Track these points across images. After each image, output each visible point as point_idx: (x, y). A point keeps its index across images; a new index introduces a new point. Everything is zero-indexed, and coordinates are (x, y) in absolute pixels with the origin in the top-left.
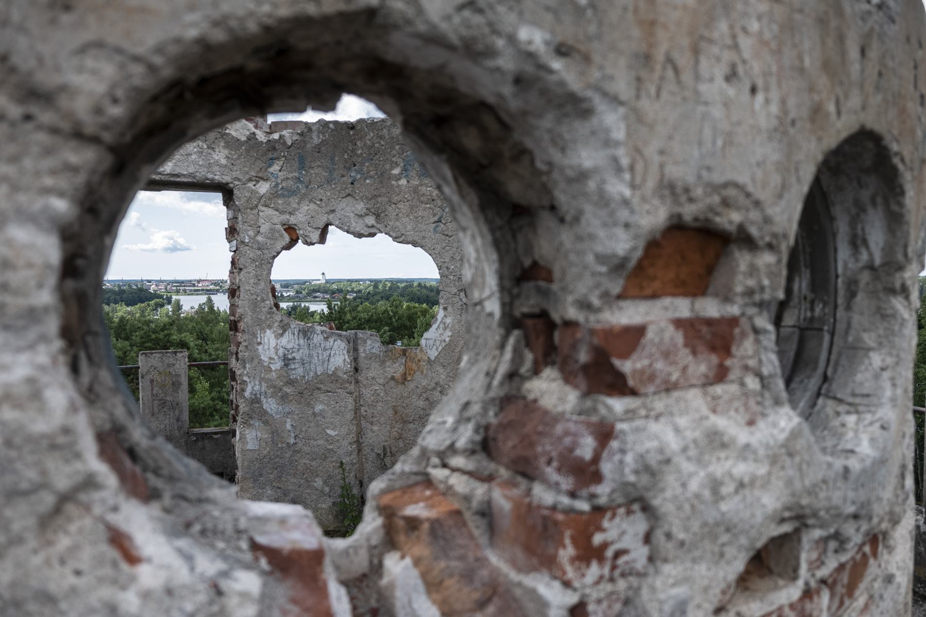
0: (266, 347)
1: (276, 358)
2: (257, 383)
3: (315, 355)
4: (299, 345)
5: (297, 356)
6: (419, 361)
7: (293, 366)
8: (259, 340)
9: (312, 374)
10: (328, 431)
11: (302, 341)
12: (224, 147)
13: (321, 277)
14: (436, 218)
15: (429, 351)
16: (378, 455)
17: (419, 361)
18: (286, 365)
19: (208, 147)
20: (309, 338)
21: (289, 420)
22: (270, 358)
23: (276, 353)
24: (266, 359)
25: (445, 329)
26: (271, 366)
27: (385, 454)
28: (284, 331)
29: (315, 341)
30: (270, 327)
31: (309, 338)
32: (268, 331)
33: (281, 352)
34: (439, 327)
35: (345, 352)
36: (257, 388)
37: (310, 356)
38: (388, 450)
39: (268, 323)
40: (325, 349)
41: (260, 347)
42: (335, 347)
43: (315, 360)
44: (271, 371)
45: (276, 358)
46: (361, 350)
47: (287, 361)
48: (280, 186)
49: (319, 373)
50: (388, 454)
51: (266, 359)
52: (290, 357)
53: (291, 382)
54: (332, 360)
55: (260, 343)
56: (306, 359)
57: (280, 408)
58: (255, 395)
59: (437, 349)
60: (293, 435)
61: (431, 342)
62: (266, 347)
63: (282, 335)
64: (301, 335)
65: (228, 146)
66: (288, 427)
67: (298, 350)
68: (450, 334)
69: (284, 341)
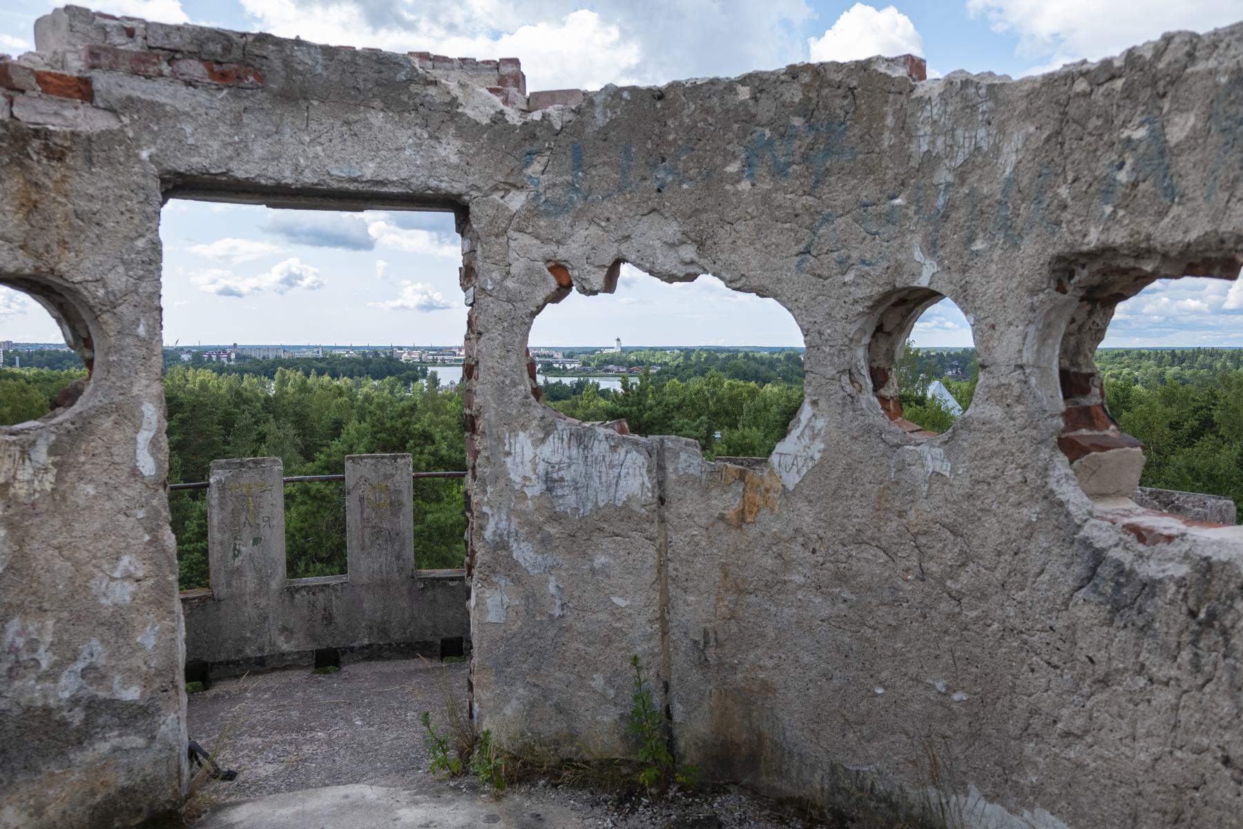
0: (518, 460)
1: (533, 477)
2: (504, 517)
3: (595, 474)
4: (570, 458)
5: (567, 475)
6: (767, 490)
7: (560, 492)
8: (507, 448)
9: (590, 505)
10: (615, 600)
11: (574, 452)
12: (456, 136)
13: (615, 345)
14: (801, 247)
15: (784, 475)
16: (695, 642)
17: (767, 490)
18: (550, 490)
19: (430, 137)
20: (586, 447)
21: (552, 578)
22: (525, 478)
23: (534, 470)
24: (518, 479)
25: (814, 437)
26: (525, 490)
27: (706, 643)
28: (547, 434)
29: (596, 451)
30: (524, 427)
31: (586, 447)
32: (521, 434)
33: (541, 468)
34: (802, 434)
35: (644, 471)
36: (503, 525)
37: (588, 476)
38: (712, 635)
39: (521, 420)
40: (612, 466)
41: (509, 460)
42: (628, 462)
43: (595, 483)
44: (526, 497)
45: (533, 477)
46: (670, 468)
47: (551, 483)
48: (543, 198)
49: (601, 504)
50: (712, 643)
51: (518, 479)
52: (555, 476)
53: (556, 518)
54: (622, 483)
55: (508, 454)
56: (581, 481)
57: (540, 558)
58: (501, 536)
59: (798, 472)
60: (558, 602)
61: (789, 460)
62: (518, 460)
63: (543, 440)
64: (573, 442)
65: (460, 134)
66: (552, 589)
67: (569, 466)
68: (822, 446)
69: (546, 450)
